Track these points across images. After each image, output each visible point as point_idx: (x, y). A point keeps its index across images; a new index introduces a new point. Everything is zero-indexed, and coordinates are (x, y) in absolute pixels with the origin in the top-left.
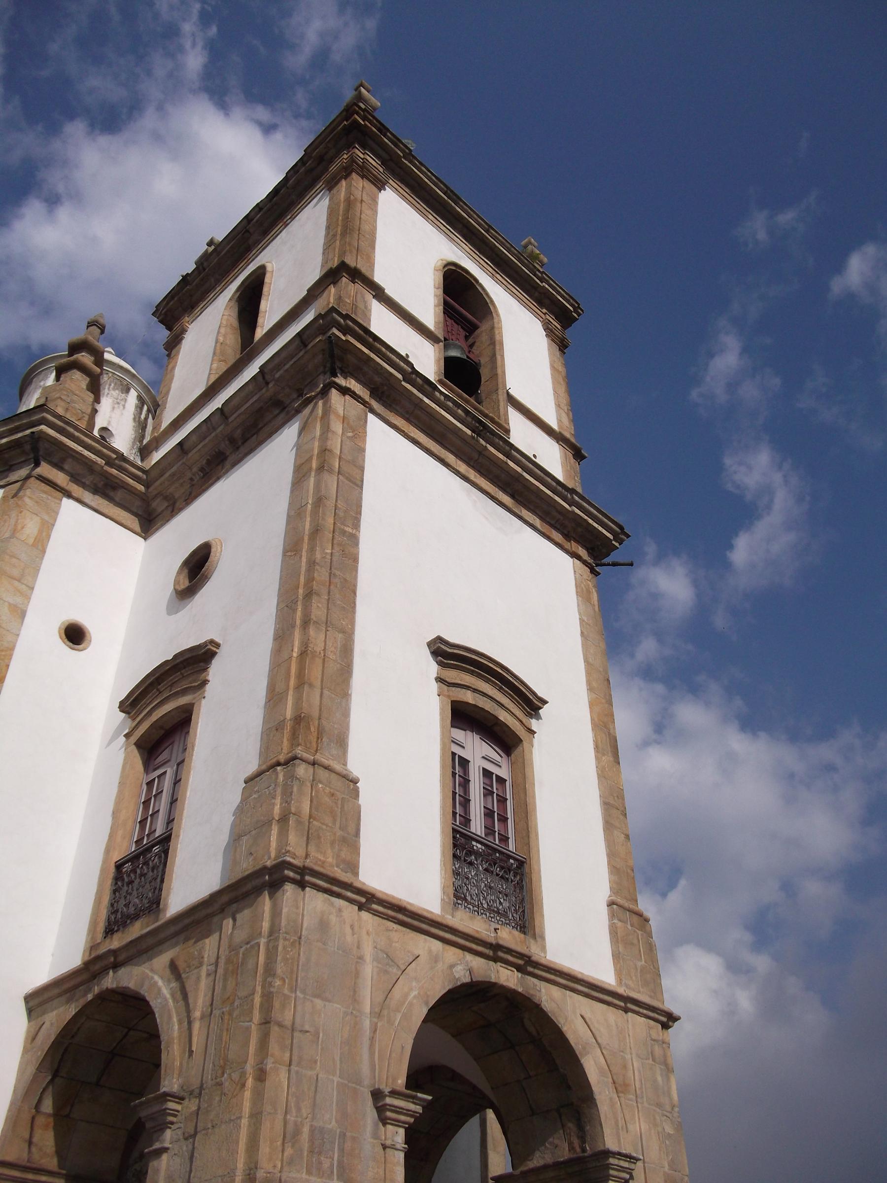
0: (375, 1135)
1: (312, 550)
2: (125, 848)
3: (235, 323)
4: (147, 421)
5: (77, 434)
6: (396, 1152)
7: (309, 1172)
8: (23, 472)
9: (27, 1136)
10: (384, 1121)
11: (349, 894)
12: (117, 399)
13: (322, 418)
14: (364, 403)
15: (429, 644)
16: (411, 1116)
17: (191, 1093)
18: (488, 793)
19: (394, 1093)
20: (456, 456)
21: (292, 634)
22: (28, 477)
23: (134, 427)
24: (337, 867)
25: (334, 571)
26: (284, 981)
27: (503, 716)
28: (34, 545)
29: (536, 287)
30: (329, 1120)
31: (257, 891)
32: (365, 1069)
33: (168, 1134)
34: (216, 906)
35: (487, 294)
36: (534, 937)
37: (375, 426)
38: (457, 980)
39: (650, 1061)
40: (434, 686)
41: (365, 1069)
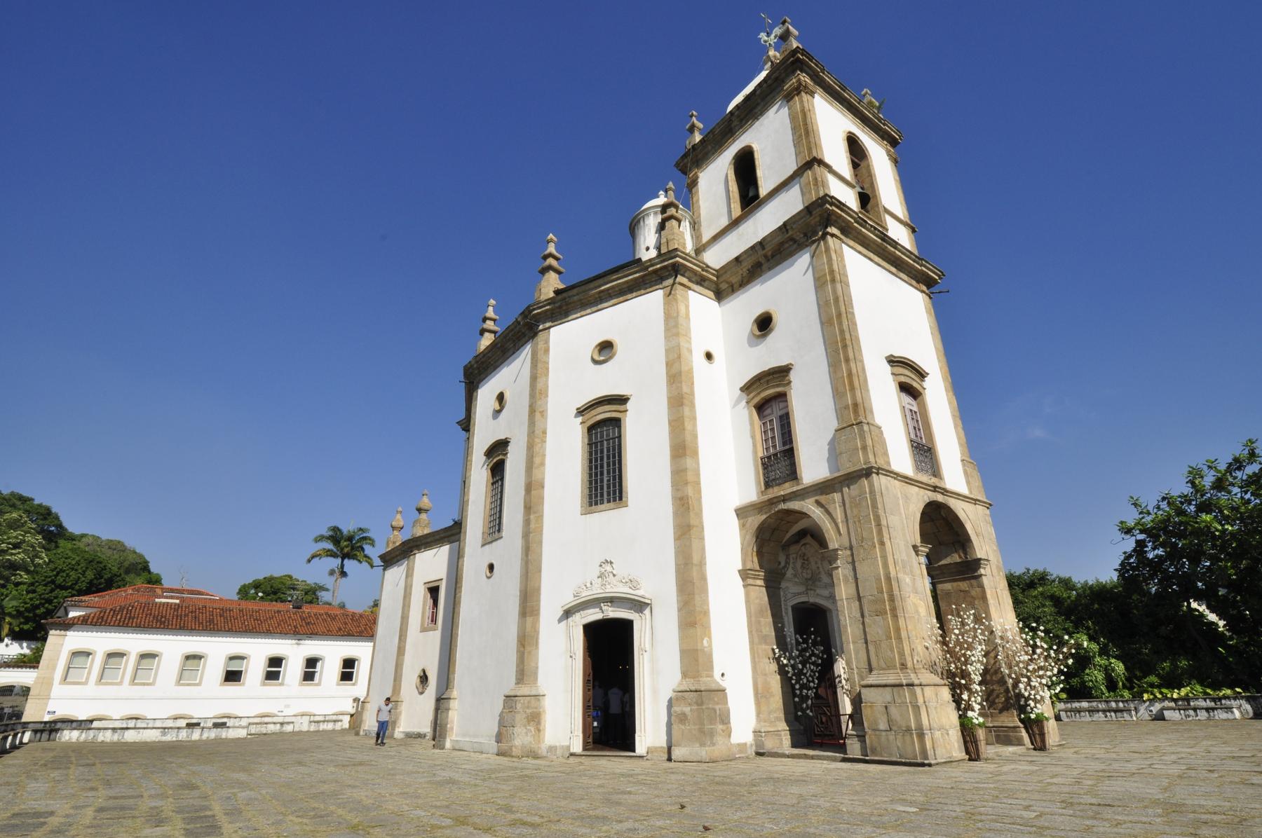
5: (690, 259)
11: (892, 475)
13: (825, 252)
14: (840, 239)
15: (886, 358)
20: (874, 253)
29: (881, 129)
30: (904, 557)
32: (909, 539)
33: (839, 561)
40: (891, 378)
41: (909, 539)
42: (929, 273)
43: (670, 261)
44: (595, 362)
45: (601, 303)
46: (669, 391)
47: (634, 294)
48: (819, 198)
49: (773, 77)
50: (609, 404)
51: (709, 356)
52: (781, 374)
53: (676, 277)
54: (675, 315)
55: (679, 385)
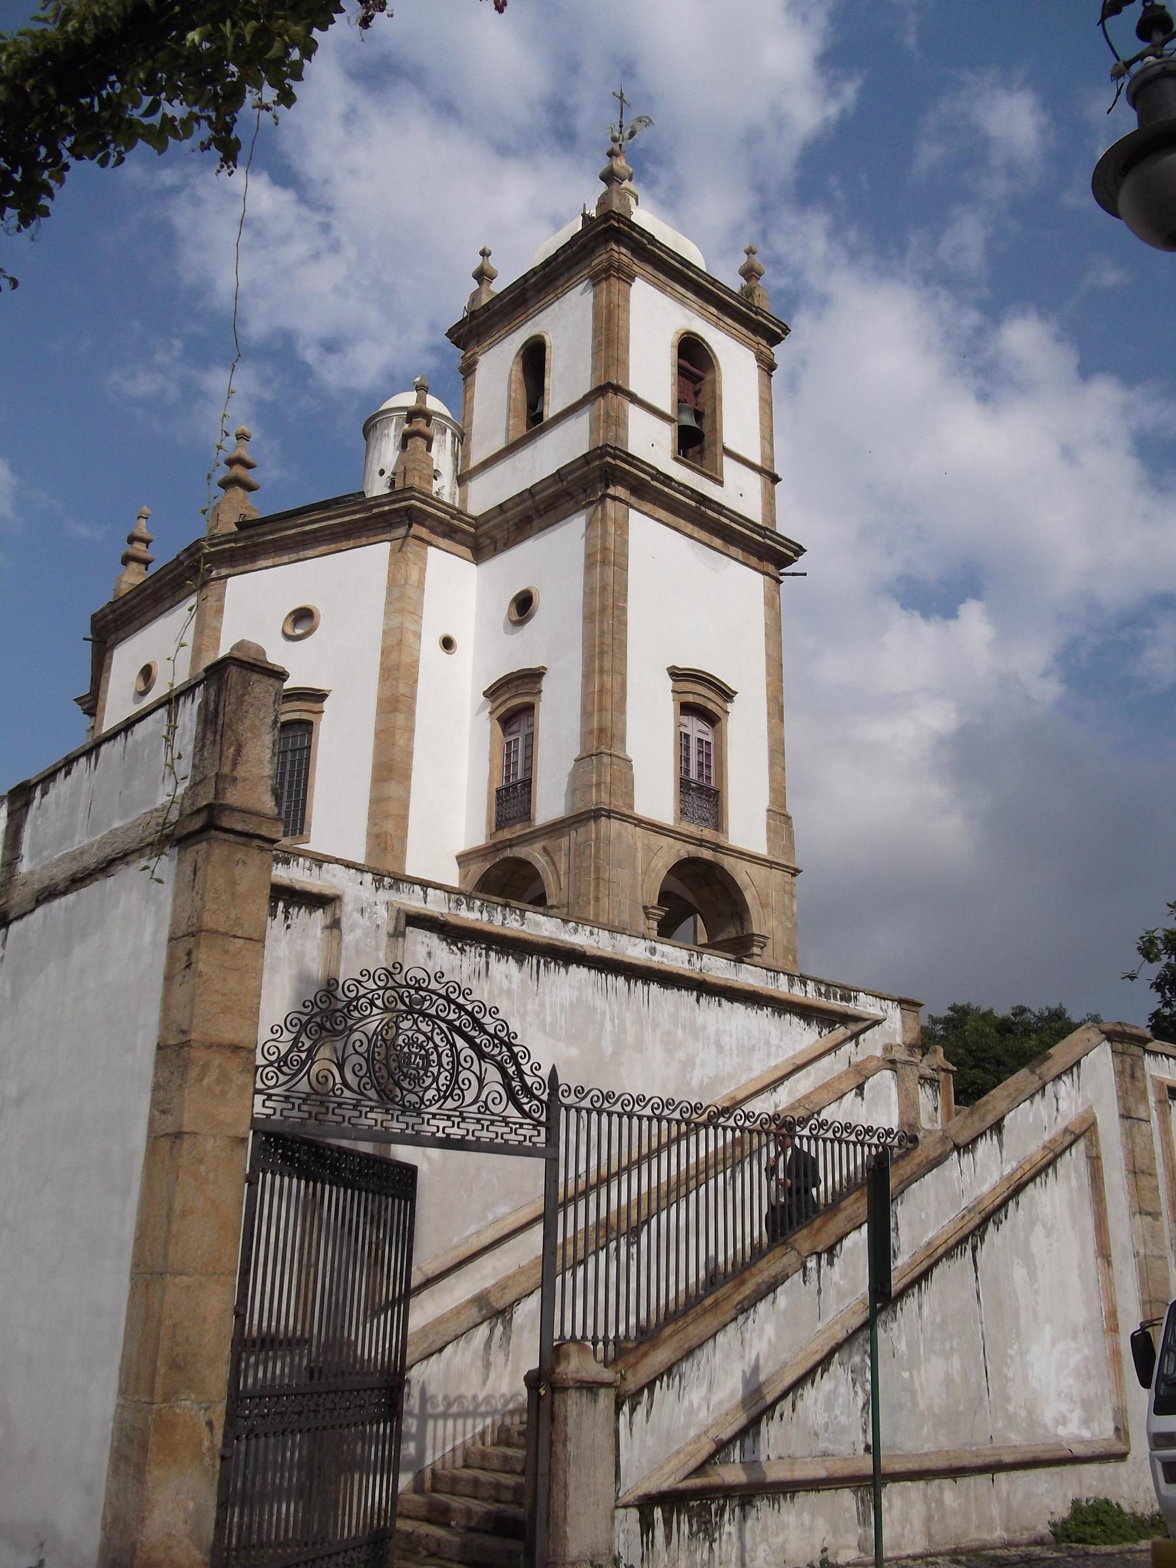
0: (645, 924)
1: (601, 622)
2: (499, 783)
3: (520, 375)
8: (401, 531)
10: (648, 918)
13: (601, 520)
14: (627, 503)
15: (668, 669)
17: (563, 905)
18: (700, 752)
19: (653, 907)
21: (594, 676)
22: (406, 537)
25: (615, 636)
27: (711, 706)
28: (418, 587)
31: (588, 819)
32: (640, 897)
34: (566, 824)
35: (711, 350)
36: (723, 832)
37: (635, 518)
41: (640, 897)
42: (778, 547)
43: (403, 504)
44: (289, 638)
45: (304, 550)
46: (381, 691)
47: (351, 543)
48: (598, 448)
49: (579, 243)
50: (300, 700)
51: (447, 643)
52: (530, 678)
53: (410, 526)
54: (402, 582)
55: (394, 683)
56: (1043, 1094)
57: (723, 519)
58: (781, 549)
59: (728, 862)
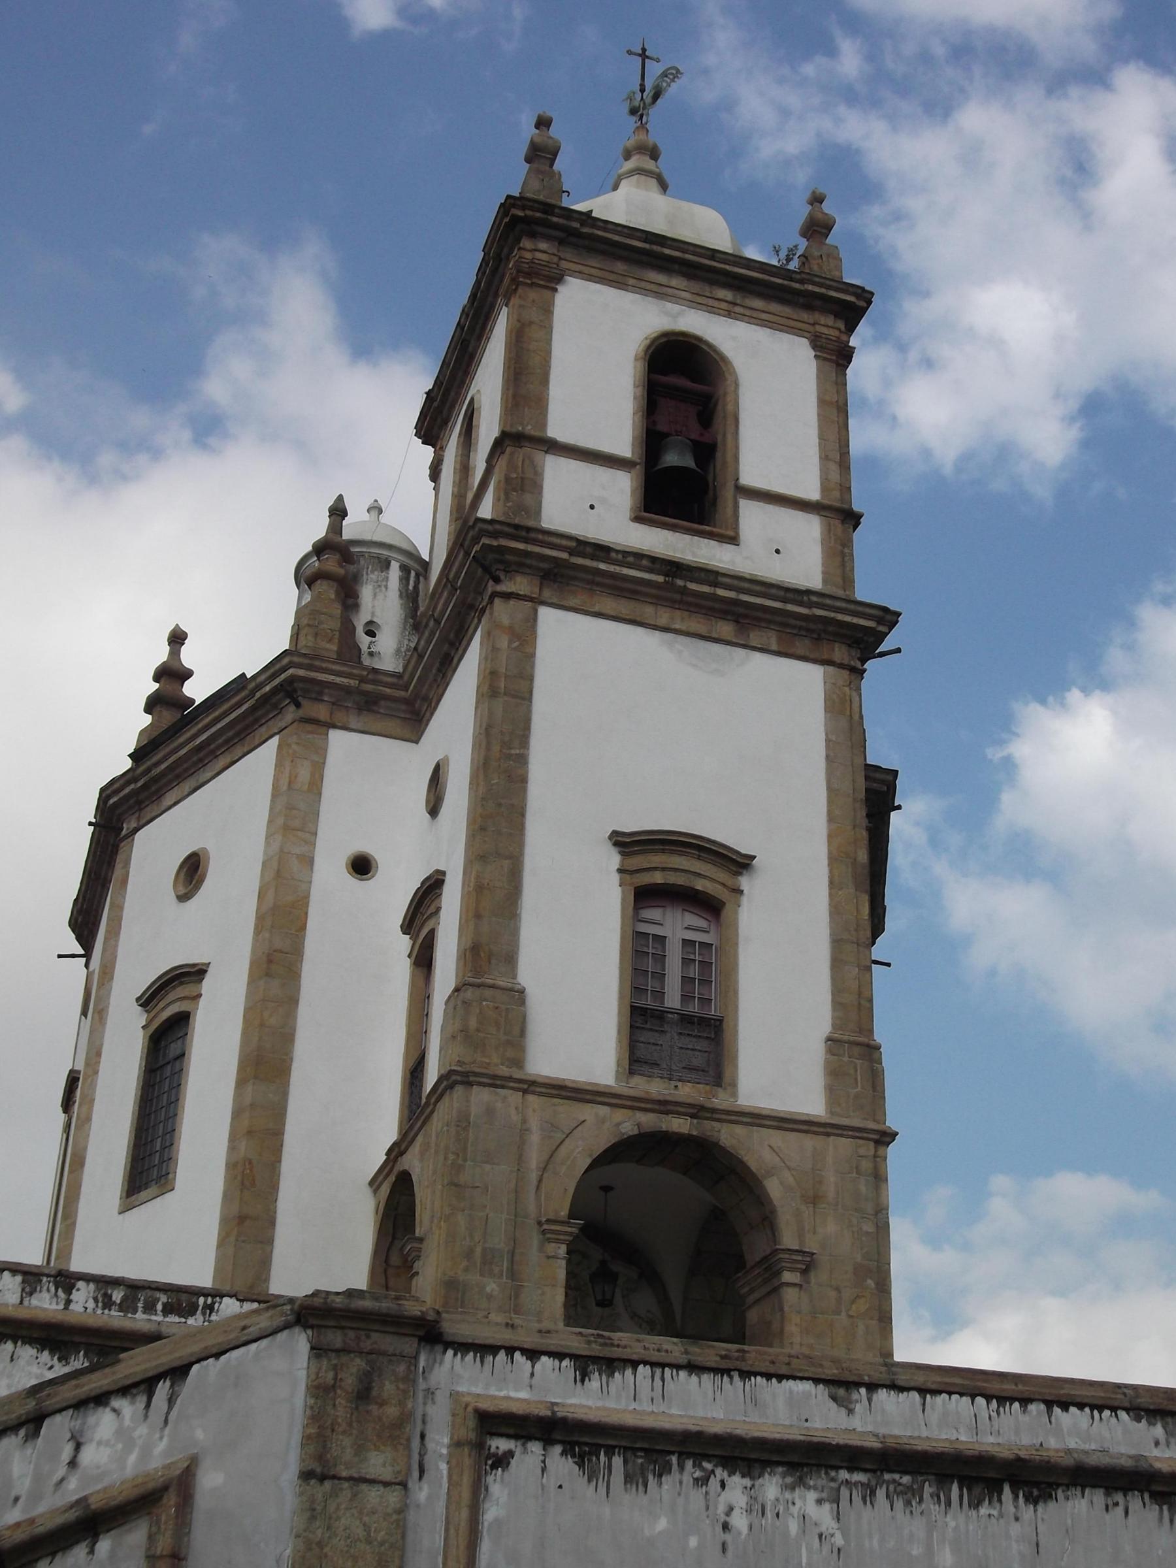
4: (418, 588)
6: (559, 1260)
7: (481, 1275)
9: (383, 1282)
12: (377, 582)
16: (571, 1236)
23: (402, 605)
24: (502, 1065)
26: (458, 1155)
38: (624, 1134)
39: (854, 1175)
43: (283, 676)
56: (36, 1433)
57: (721, 592)
58: (848, 619)
59: (728, 1136)
